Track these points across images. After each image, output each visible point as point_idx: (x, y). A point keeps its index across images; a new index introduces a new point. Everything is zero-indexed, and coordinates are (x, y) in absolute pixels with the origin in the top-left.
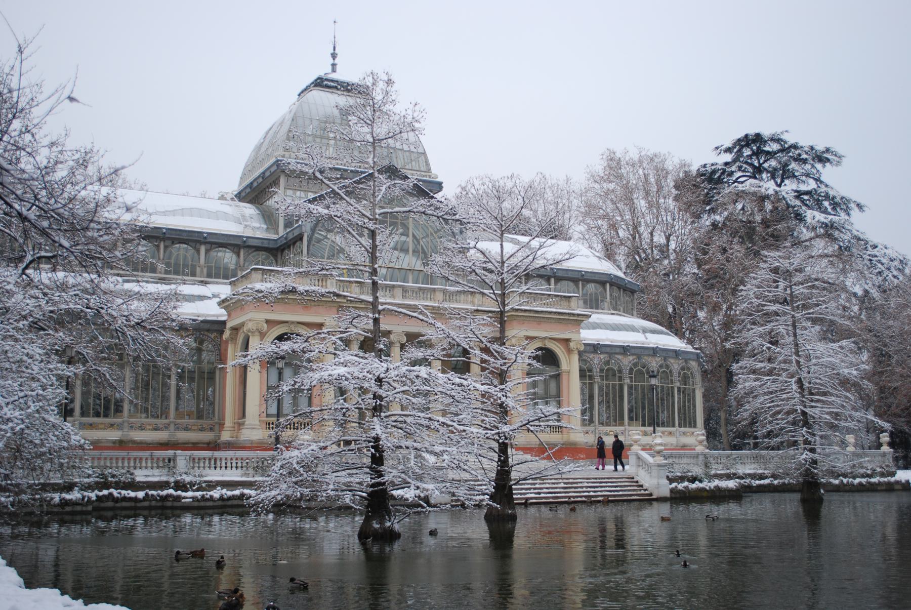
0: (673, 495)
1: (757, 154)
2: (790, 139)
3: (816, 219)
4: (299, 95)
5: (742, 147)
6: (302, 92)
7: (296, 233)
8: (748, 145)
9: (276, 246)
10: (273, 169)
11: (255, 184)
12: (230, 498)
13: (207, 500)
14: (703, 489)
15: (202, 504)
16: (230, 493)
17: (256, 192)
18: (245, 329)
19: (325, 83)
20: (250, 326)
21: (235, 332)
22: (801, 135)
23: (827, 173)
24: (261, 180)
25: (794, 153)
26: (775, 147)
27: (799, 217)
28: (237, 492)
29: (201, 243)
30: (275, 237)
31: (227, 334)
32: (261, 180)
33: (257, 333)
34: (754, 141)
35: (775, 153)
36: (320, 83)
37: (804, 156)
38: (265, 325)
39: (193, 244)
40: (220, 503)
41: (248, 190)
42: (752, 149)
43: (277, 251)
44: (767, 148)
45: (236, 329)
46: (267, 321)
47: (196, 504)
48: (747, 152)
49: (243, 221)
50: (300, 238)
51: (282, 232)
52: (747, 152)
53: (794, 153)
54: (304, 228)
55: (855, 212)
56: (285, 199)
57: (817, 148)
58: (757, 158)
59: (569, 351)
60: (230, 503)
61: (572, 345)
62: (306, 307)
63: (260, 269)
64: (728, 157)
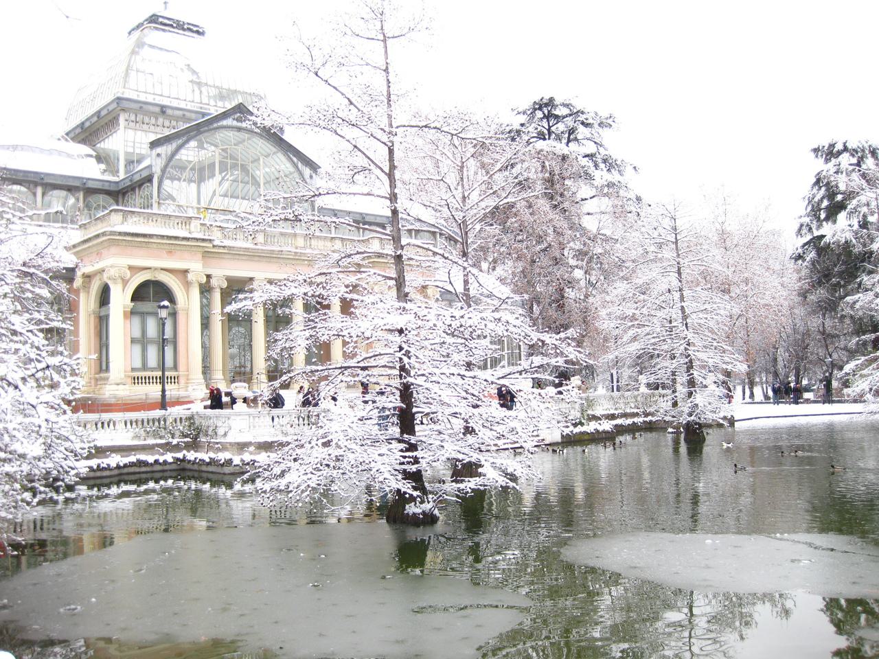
0: (565, 440)
1: (548, 117)
2: (578, 106)
3: (604, 179)
4: (130, 33)
5: (535, 109)
6: (133, 30)
7: (145, 174)
8: (540, 109)
9: (117, 189)
10: (111, 108)
11: (87, 124)
12: (125, 466)
13: (104, 469)
14: (585, 433)
15: (99, 474)
16: (126, 460)
17: (90, 132)
18: (105, 275)
19: (161, 20)
20: (113, 272)
21: (87, 280)
22: (589, 104)
23: (606, 135)
24: (95, 119)
25: (582, 118)
26: (565, 111)
27: (588, 177)
28: (133, 459)
29: (36, 184)
30: (116, 179)
31: (78, 282)
32: (95, 119)
33: (120, 281)
34: (546, 105)
35: (564, 117)
36: (153, 19)
37: (590, 121)
38: (128, 272)
39: (27, 185)
40: (116, 472)
41: (79, 130)
42: (544, 113)
43: (119, 194)
44: (557, 112)
45: (88, 277)
46: (130, 268)
47: (92, 474)
48: (539, 114)
49: (81, 164)
50: (149, 179)
51: (122, 175)
52: (539, 114)
53: (582, 118)
54: (154, 169)
55: (629, 171)
56: (127, 141)
57: (600, 114)
58: (548, 121)
59: (187, 284)
60: (126, 470)
61: (190, 276)
62: (170, 252)
63: (121, 210)
64: (523, 119)
